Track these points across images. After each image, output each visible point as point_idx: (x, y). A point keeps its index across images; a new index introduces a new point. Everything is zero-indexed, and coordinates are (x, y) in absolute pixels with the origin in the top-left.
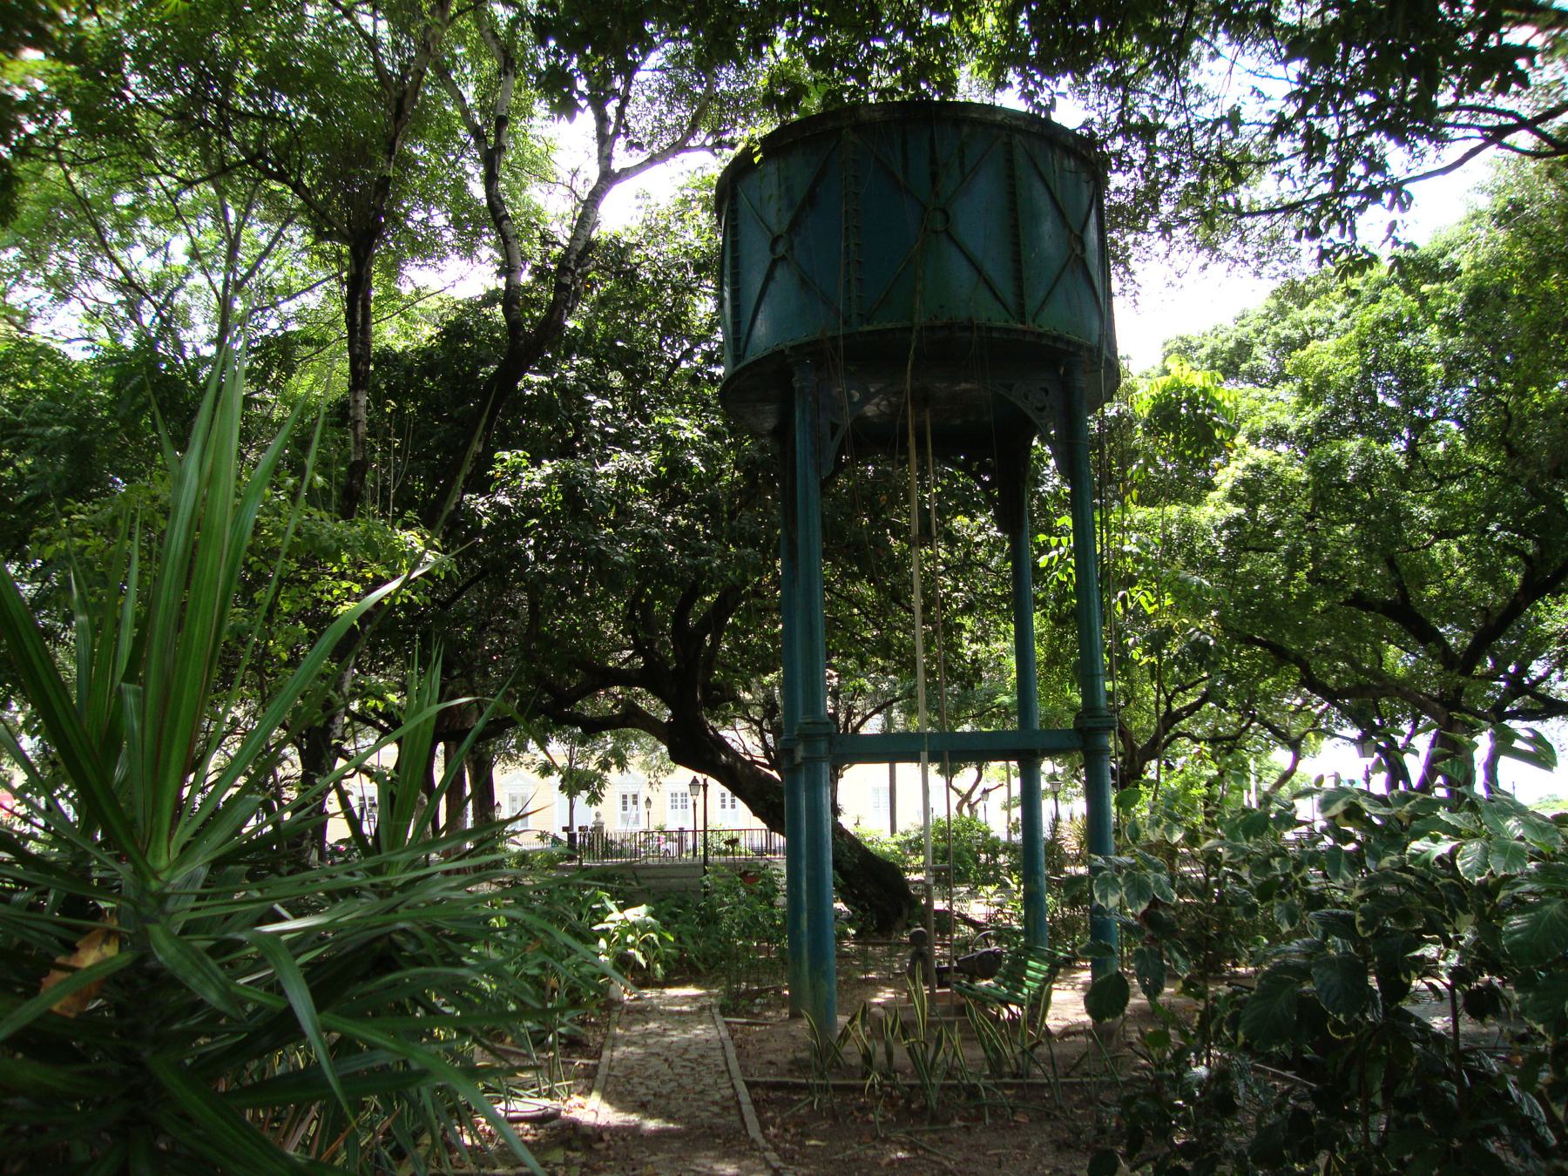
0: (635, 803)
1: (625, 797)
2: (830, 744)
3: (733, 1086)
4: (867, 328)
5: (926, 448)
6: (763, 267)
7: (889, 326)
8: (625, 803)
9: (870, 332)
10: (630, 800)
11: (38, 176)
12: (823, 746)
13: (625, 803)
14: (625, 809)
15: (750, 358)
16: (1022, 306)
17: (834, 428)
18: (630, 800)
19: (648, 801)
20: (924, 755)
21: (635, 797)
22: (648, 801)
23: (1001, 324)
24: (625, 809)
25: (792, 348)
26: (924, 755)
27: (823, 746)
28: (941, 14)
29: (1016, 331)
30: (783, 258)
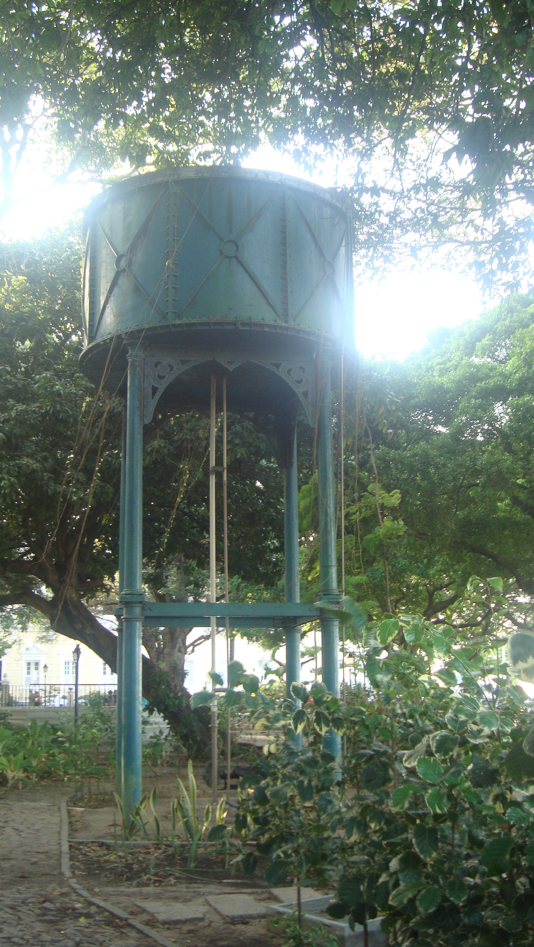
0: (37, 669)
1: (29, 664)
2: (143, 609)
3: (59, 844)
4: (178, 322)
5: (222, 405)
6: (111, 275)
7: (194, 321)
8: (29, 669)
9: (180, 325)
10: (33, 667)
11: (472, 116)
12: (137, 610)
13: (29, 669)
14: (29, 673)
15: (99, 340)
16: (286, 310)
17: (155, 390)
18: (33, 667)
19: (45, 667)
20: (213, 620)
21: (37, 664)
22: (45, 667)
23: (272, 323)
24: (29, 673)
25: (126, 334)
26: (213, 620)
27: (137, 610)
28: (424, 99)
29: (281, 327)
30: (124, 270)
